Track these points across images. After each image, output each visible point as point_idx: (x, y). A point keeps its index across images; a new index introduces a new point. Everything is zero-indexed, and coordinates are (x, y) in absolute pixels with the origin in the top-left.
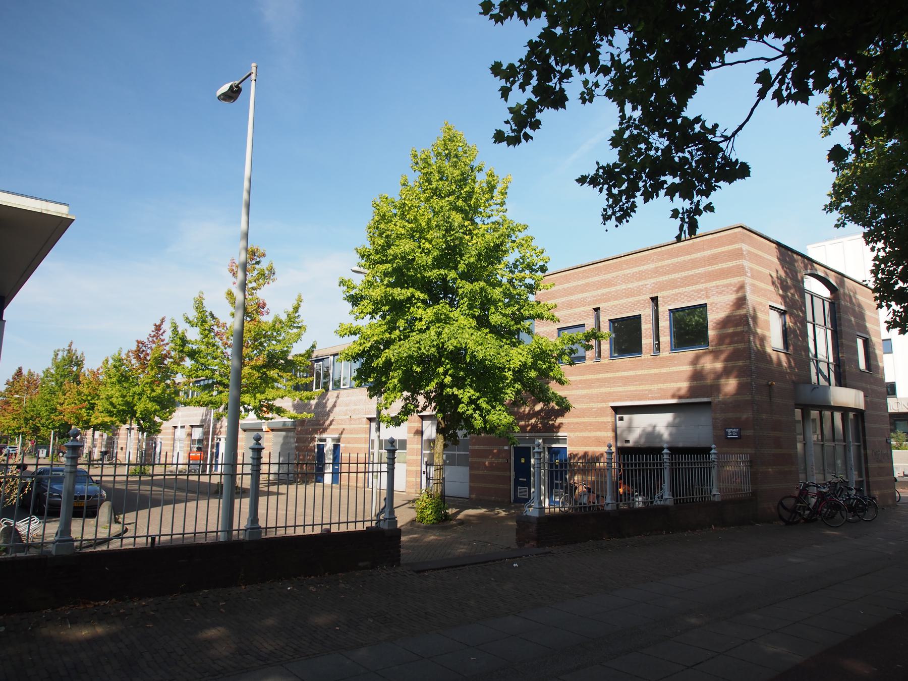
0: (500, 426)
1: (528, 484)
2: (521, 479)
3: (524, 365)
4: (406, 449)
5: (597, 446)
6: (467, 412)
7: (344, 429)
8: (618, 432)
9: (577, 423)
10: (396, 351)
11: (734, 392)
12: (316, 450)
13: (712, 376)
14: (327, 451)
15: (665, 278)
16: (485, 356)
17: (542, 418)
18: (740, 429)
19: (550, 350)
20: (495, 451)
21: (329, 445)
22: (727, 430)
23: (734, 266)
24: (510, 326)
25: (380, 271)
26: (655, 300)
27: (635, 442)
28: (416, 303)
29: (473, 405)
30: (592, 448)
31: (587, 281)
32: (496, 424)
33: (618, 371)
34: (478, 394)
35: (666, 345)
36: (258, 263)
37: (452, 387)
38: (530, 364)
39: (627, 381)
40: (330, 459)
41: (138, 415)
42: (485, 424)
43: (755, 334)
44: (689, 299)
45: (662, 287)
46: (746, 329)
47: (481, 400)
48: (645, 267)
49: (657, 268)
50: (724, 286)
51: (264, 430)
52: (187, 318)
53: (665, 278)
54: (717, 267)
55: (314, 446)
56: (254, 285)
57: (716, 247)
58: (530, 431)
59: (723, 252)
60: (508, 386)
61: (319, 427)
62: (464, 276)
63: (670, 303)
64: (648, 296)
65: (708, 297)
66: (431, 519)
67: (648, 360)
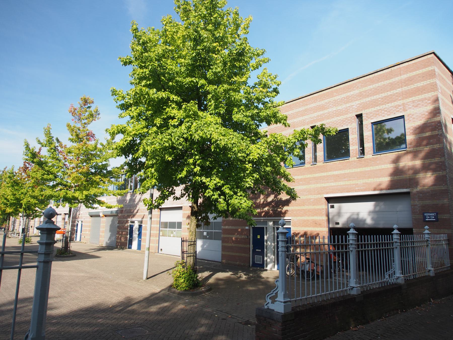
0: (240, 209)
1: (262, 254)
2: (257, 250)
3: (261, 158)
4: (181, 228)
5: (314, 227)
6: (213, 197)
7: (144, 215)
8: (330, 217)
9: (299, 210)
10: (149, 141)
11: (432, 184)
12: (129, 228)
13: (411, 172)
14: (135, 229)
15: (368, 99)
16: (227, 144)
17: (273, 206)
18: (437, 214)
19: (284, 143)
20: (239, 230)
21: (136, 225)
22: (425, 214)
23: (428, 84)
24: (250, 125)
25: (137, 73)
26: (359, 116)
27: (343, 224)
28: (170, 105)
29: (219, 192)
30: (310, 228)
31: (306, 107)
32: (236, 207)
33: (331, 171)
34: (222, 182)
35: (369, 150)
36: (89, 107)
37: (201, 176)
38: (267, 157)
39: (337, 178)
40: (136, 234)
41: (23, 206)
42: (228, 207)
43: (446, 138)
44: (389, 113)
45: (366, 106)
46: (440, 133)
47: (225, 187)
48: (352, 93)
49: (361, 93)
50: (419, 100)
51: (101, 216)
52: (39, 141)
53: (368, 99)
54: (412, 87)
55: (128, 226)
56: (86, 121)
57: (410, 72)
58: (264, 216)
59: (418, 75)
60: (248, 175)
61: (130, 214)
62: (210, 82)
63: (372, 117)
64: (354, 114)
65: (405, 110)
66: (184, 286)
67: (354, 161)
